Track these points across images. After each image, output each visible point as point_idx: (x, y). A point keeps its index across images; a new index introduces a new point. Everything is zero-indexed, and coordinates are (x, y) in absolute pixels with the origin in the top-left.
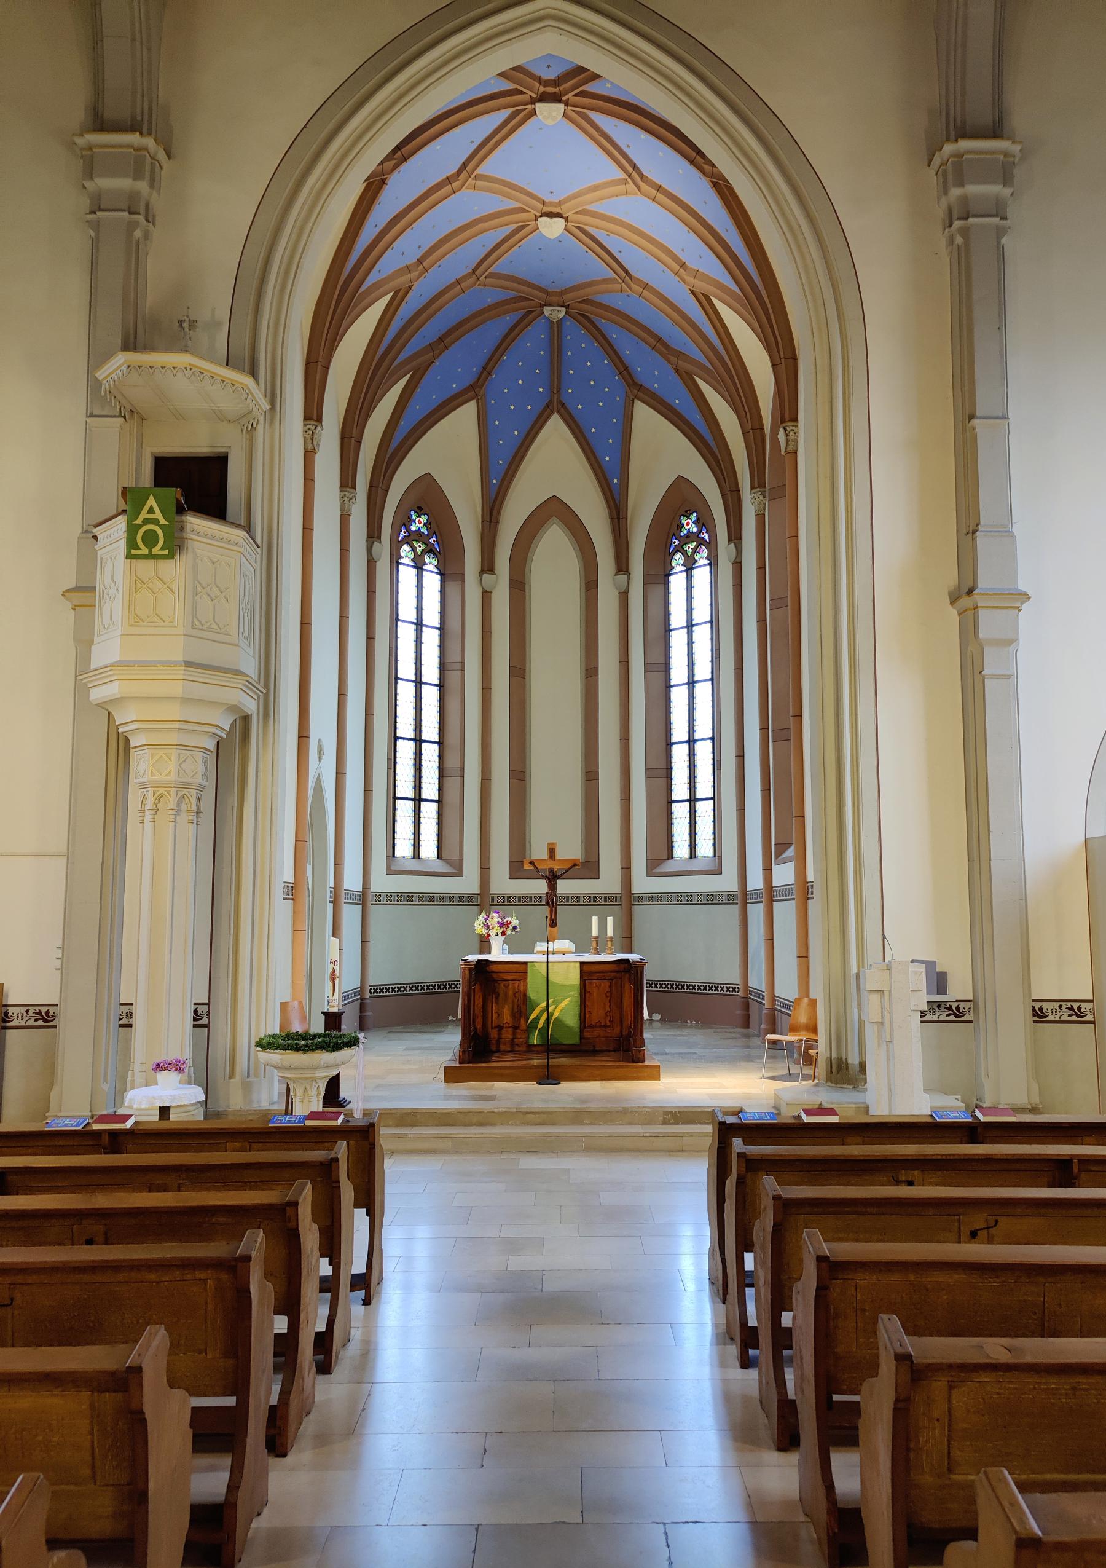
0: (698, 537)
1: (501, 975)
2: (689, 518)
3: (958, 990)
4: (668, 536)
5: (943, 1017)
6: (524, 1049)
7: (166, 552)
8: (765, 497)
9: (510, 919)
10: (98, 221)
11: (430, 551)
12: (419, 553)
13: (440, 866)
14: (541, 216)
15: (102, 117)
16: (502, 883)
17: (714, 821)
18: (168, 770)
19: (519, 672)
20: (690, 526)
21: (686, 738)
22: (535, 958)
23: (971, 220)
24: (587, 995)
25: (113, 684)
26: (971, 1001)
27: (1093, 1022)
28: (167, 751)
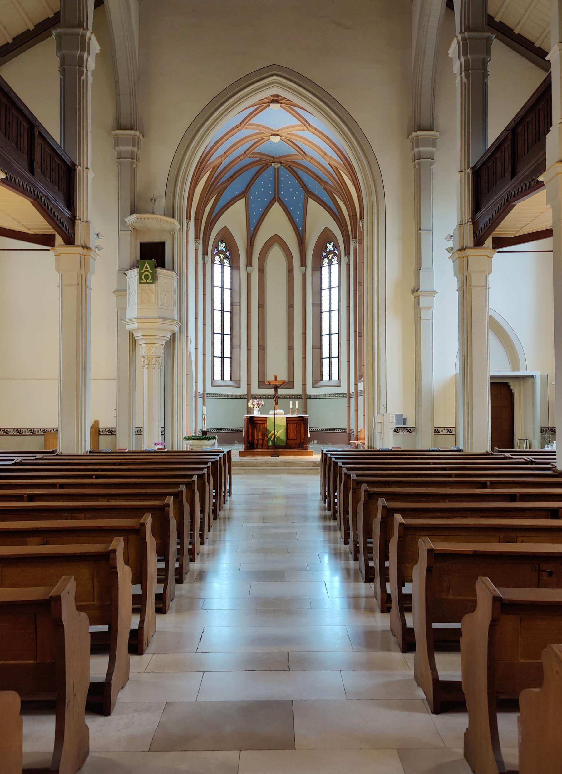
0: (333, 252)
1: (258, 421)
2: (330, 244)
3: (410, 424)
4: (322, 251)
5: (405, 433)
6: (266, 447)
7: (152, 281)
8: (357, 242)
9: (261, 402)
10: (121, 161)
11: (227, 257)
12: (222, 259)
13: (232, 383)
14: (271, 135)
15: (120, 124)
16: (256, 390)
17: (339, 366)
18: (152, 351)
19: (262, 306)
20: (330, 248)
21: (328, 333)
22: (271, 415)
23: (421, 160)
24: (288, 429)
25: (136, 324)
26: (414, 427)
27: (455, 434)
28: (152, 346)
